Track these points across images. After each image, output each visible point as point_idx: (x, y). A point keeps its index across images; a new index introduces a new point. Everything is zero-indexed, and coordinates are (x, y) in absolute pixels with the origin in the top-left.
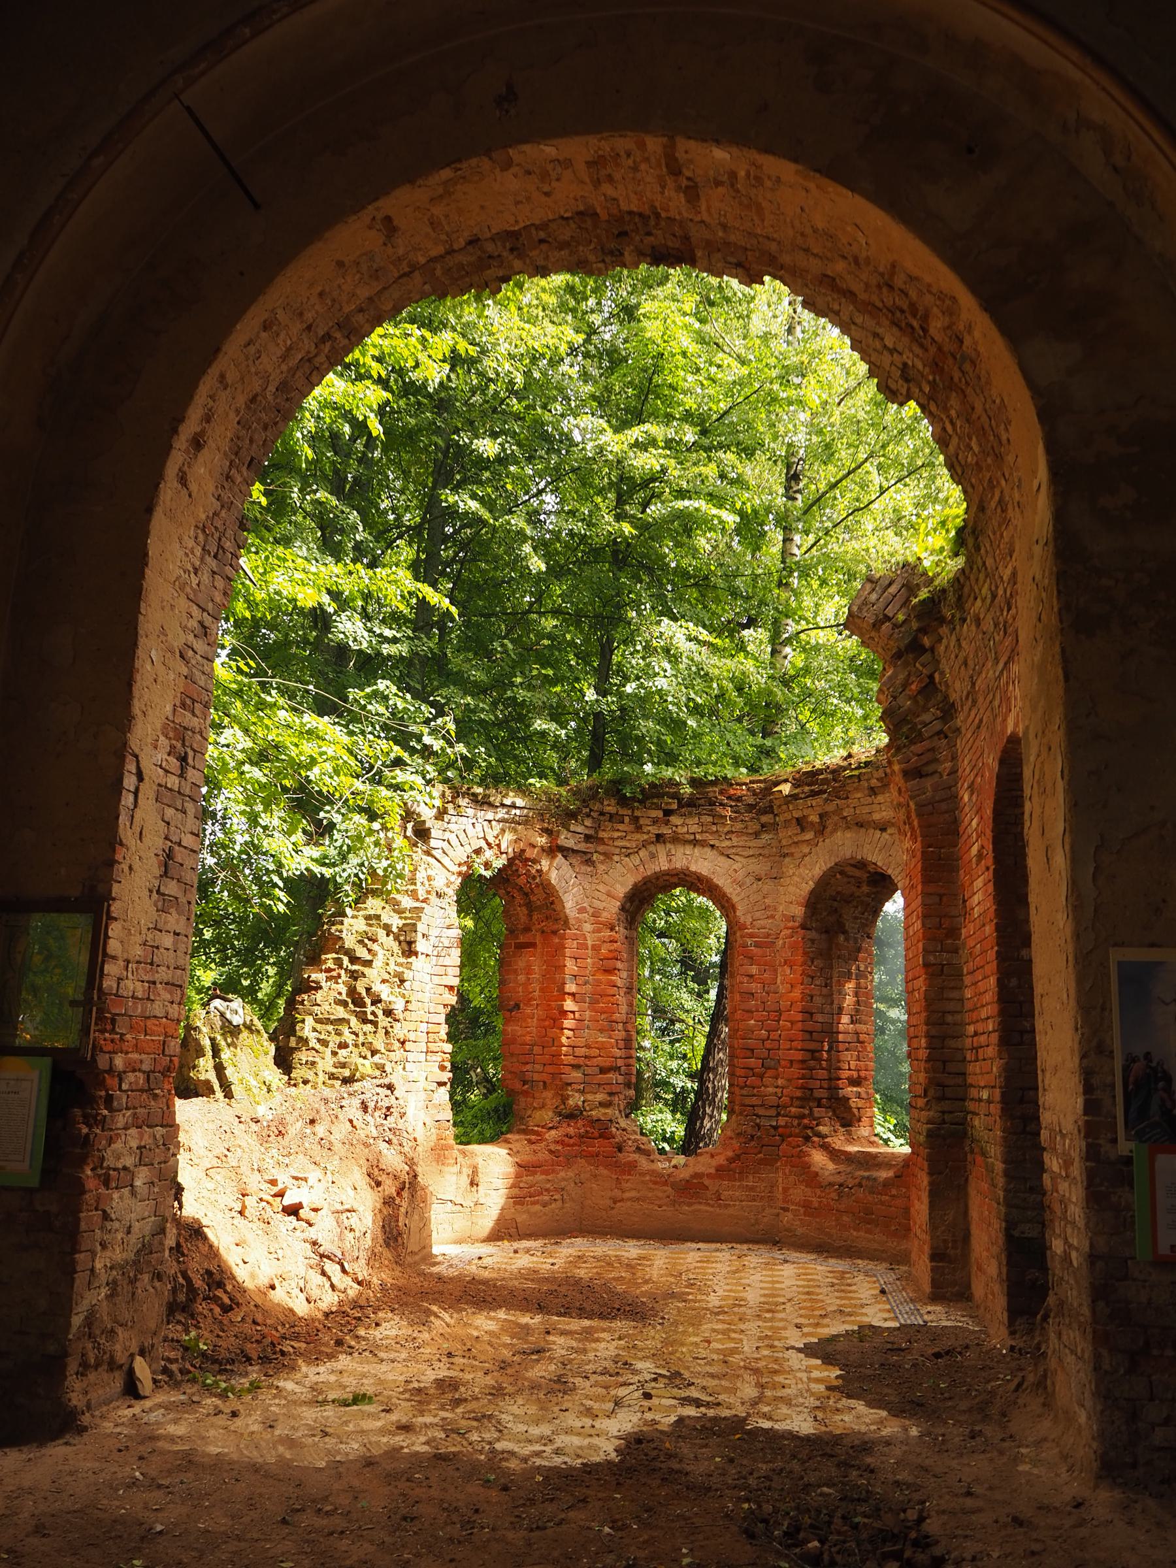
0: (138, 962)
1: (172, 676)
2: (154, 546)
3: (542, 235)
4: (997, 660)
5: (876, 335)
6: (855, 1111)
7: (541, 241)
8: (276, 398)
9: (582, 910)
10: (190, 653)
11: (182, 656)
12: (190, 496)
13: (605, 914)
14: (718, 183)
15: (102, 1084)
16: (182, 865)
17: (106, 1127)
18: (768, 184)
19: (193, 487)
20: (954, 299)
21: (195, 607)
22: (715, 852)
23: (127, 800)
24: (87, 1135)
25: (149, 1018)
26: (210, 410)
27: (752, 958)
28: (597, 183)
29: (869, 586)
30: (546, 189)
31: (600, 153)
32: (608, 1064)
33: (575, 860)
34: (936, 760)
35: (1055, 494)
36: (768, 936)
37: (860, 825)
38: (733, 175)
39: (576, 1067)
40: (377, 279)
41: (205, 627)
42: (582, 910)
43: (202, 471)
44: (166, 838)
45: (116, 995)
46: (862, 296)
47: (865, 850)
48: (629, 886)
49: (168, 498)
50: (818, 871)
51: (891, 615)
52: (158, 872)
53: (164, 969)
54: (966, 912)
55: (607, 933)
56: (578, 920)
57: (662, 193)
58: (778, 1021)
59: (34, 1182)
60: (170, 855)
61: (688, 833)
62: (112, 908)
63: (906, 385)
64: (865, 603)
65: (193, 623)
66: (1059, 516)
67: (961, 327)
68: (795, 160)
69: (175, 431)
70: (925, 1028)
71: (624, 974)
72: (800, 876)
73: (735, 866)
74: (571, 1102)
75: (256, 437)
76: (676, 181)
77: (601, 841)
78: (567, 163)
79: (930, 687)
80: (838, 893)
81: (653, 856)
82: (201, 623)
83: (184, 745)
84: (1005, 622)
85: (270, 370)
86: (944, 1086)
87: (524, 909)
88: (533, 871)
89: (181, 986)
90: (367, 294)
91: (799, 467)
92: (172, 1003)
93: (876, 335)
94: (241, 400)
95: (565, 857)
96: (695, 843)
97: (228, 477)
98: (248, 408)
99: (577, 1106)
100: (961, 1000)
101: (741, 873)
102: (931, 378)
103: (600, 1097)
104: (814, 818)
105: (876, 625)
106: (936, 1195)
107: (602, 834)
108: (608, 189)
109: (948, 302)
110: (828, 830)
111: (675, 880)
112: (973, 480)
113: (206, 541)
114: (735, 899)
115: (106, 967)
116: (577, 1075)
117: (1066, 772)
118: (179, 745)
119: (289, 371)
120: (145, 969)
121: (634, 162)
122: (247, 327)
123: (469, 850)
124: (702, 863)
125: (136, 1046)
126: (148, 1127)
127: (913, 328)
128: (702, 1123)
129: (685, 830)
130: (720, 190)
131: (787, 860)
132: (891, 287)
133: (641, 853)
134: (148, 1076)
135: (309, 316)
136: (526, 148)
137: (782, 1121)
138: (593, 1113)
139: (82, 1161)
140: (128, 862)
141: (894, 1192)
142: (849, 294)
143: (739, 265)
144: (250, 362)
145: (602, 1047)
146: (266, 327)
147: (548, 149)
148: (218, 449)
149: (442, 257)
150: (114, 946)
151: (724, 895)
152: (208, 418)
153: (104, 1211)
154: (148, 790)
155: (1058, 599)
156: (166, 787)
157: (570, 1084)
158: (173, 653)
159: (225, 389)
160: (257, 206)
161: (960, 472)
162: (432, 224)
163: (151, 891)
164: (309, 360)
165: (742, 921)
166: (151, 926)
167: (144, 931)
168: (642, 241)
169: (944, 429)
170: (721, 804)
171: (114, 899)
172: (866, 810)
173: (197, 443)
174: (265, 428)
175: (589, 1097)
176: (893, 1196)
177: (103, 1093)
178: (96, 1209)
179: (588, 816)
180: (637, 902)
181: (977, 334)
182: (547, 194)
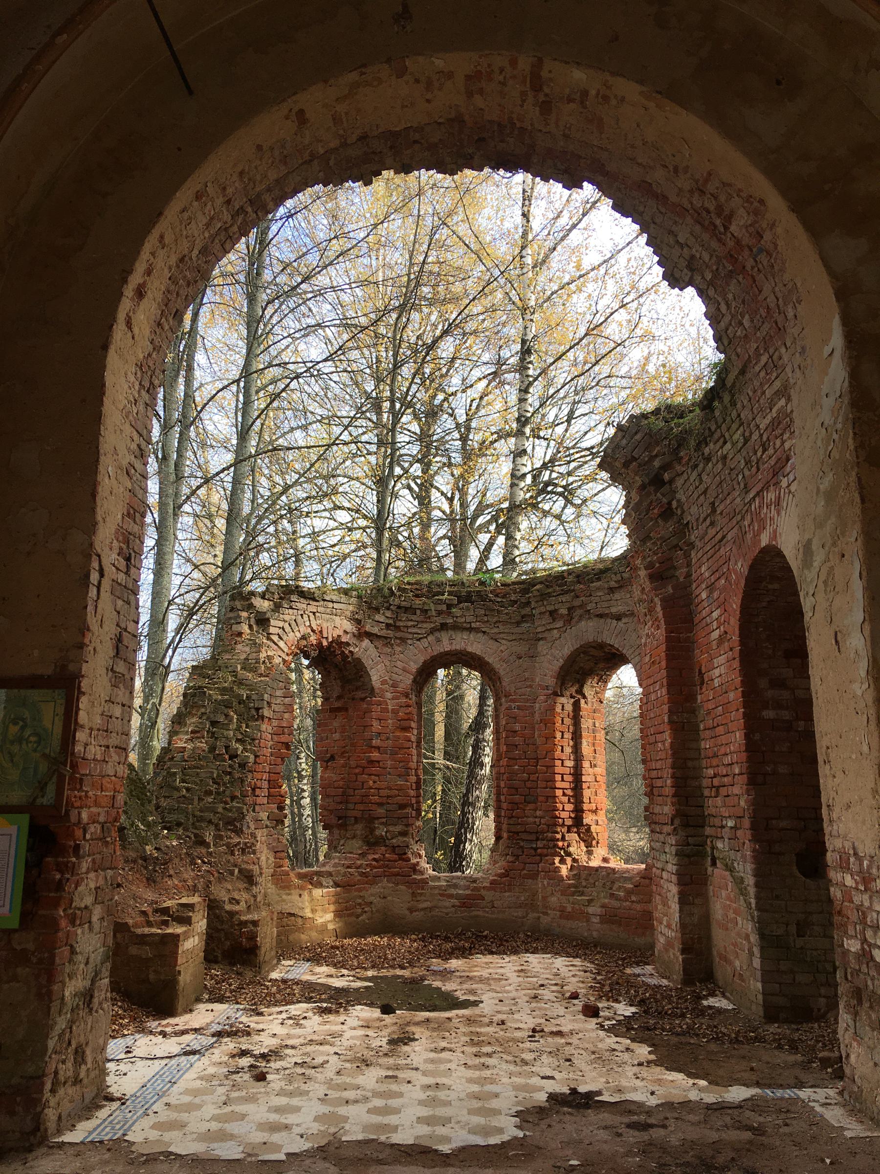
0: (99, 730)
1: (122, 489)
2: (109, 378)
3: (417, 136)
4: (746, 489)
5: (671, 232)
6: (595, 835)
7: (415, 142)
8: (199, 259)
9: (384, 682)
10: (133, 471)
11: (127, 473)
12: (133, 338)
13: (402, 685)
14: (570, 100)
15: (71, 836)
16: (127, 647)
17: (75, 872)
18: (614, 102)
19: (136, 330)
20: (762, 202)
21: (135, 433)
22: (486, 636)
23: (93, 592)
24: (60, 880)
25: (103, 777)
26: (151, 265)
27: (515, 718)
28: (470, 95)
29: (620, 434)
30: (429, 96)
31: (479, 68)
32: (405, 802)
34: (675, 568)
35: (850, 358)
36: (527, 701)
37: (600, 616)
38: (585, 93)
39: (381, 805)
40: (285, 163)
41: (141, 450)
42: (384, 682)
43: (142, 317)
44: (118, 625)
45: (83, 759)
46: (673, 198)
47: (604, 636)
49: (119, 339)
50: (567, 651)
51: (637, 456)
52: (112, 653)
53: (115, 735)
56: (382, 690)
57: (522, 106)
58: (536, 766)
59: (15, 924)
60: (119, 640)
61: (465, 622)
62: (82, 684)
63: (689, 274)
64: (617, 446)
65: (134, 446)
66: (854, 375)
67: (764, 226)
68: (641, 82)
69: (125, 281)
70: (670, 771)
71: (415, 732)
72: (552, 655)
73: (501, 648)
74: (377, 832)
75: (181, 292)
76: (535, 97)
77: (398, 628)
78: (450, 75)
79: (667, 513)
80: (581, 668)
81: (439, 640)
82: (139, 446)
83: (128, 547)
84: (758, 461)
85: (196, 235)
86: (687, 816)
87: (338, 681)
88: (347, 652)
89: (125, 749)
90: (275, 176)
91: (532, 344)
92: (119, 763)
93: (671, 232)
94: (173, 260)
95: (371, 641)
96: (471, 630)
97: (159, 324)
98: (178, 266)
99: (382, 836)
100: (698, 750)
101: (505, 654)
102: (715, 267)
103: (399, 828)
104: (564, 611)
105: (626, 465)
107: (399, 624)
108: (479, 101)
109: (756, 204)
110: (574, 620)
111: (453, 659)
112: (739, 350)
113: (142, 377)
114: (502, 673)
115: (77, 734)
116: (381, 811)
117: (864, 574)
118: (124, 546)
119: (211, 236)
120: (102, 736)
121: (505, 78)
122: (183, 196)
123: (299, 635)
124: (475, 645)
125: (96, 801)
126: (102, 870)
127: (715, 226)
128: (464, 846)
129: (463, 620)
130: (572, 106)
131: (541, 642)
132: (702, 192)
133: (429, 638)
134: (103, 827)
135: (230, 191)
136: (421, 59)
137: (540, 844)
138: (394, 841)
139: (56, 904)
140: (93, 645)
141: (634, 898)
142: (662, 199)
143: (566, 171)
144: (183, 226)
145: (400, 789)
146: (198, 196)
147: (438, 62)
148: (154, 300)
149: (337, 149)
150: (83, 717)
151: (493, 669)
152: (149, 272)
153: (72, 946)
154: (106, 584)
155: (854, 439)
156: (117, 582)
157: (378, 818)
158: (122, 470)
159: (163, 248)
160: (190, 92)
161: (726, 343)
162: (334, 119)
163: (107, 669)
164: (226, 229)
165: (507, 689)
166: (108, 699)
167: (103, 703)
168: (495, 147)
169: (718, 309)
170: (490, 600)
171: (83, 676)
172: (605, 604)
173: (140, 293)
174: (188, 285)
175: (391, 828)
176: (633, 902)
177: (72, 843)
178: (66, 945)
179: (388, 609)
180: (424, 676)
181: (779, 230)
182: (428, 101)
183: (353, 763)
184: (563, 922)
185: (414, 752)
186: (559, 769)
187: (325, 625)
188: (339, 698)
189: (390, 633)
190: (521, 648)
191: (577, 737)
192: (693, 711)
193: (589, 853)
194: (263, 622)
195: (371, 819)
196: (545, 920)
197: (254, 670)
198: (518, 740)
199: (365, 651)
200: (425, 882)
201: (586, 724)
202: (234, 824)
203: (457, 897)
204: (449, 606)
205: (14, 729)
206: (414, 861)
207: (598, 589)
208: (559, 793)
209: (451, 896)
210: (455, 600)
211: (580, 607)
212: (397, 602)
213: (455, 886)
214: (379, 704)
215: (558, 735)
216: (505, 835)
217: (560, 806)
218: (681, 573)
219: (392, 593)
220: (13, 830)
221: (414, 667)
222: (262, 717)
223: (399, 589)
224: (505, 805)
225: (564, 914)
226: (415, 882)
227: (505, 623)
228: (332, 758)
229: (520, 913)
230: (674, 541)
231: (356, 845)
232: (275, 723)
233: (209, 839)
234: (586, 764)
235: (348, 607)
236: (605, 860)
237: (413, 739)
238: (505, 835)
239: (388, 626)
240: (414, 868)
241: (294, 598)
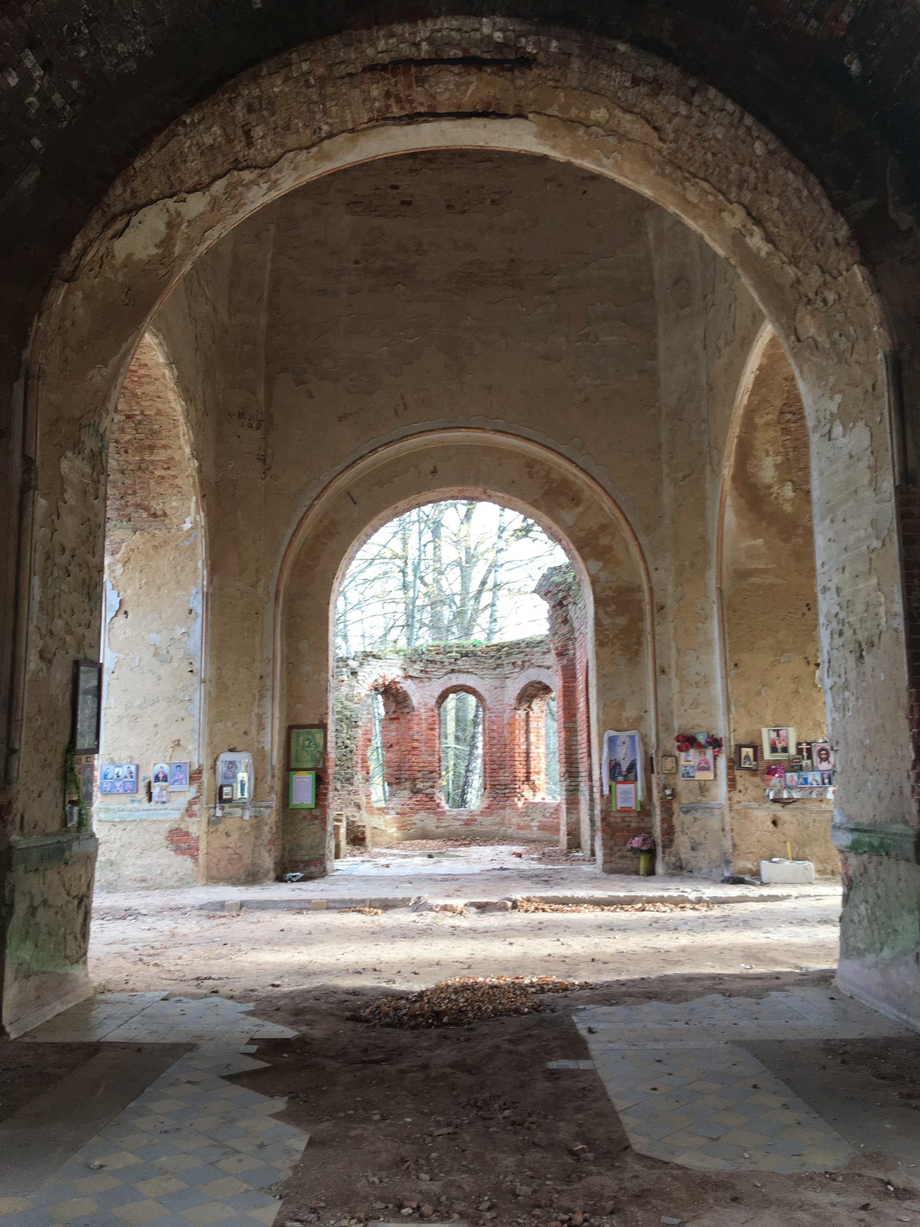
9: (420, 703)
33: (416, 681)
37: (539, 666)
42: (420, 703)
48: (439, 693)
54: (578, 709)
55: (431, 713)
59: (313, 806)
74: (418, 786)
77: (427, 672)
79: (566, 621)
81: (450, 679)
96: (468, 672)
103: (430, 784)
104: (519, 663)
106: (568, 811)
116: (419, 775)
137: (507, 791)
160: (355, 503)
183: (403, 749)
184: (519, 831)
185: (437, 741)
186: (517, 750)
187: (387, 673)
188: (395, 712)
189: (422, 675)
190: (496, 683)
191: (527, 732)
192: (575, 722)
193: (534, 795)
194: (354, 673)
195: (415, 779)
196: (510, 831)
197: (351, 701)
198: (495, 734)
199: (408, 686)
200: (444, 812)
201: (533, 725)
202: (349, 780)
203: (462, 820)
204: (456, 660)
205: (307, 743)
206: (438, 801)
207: (537, 652)
208: (517, 763)
209: (458, 820)
210: (459, 656)
211: (529, 661)
212: (426, 658)
213: (461, 815)
214: (417, 715)
215: (517, 732)
216: (488, 787)
217: (517, 770)
218: (571, 652)
219: (423, 653)
220: (310, 776)
221: (437, 694)
222: (358, 726)
223: (428, 650)
224: (488, 771)
225: (520, 827)
226: (439, 812)
227: (487, 669)
228: (391, 746)
229: (496, 827)
230: (568, 636)
231: (407, 793)
232: (363, 728)
233: (339, 788)
234: (533, 747)
235: (399, 661)
236: (543, 799)
237: (437, 734)
238: (488, 787)
239: (422, 671)
240: (438, 805)
241: (370, 658)
